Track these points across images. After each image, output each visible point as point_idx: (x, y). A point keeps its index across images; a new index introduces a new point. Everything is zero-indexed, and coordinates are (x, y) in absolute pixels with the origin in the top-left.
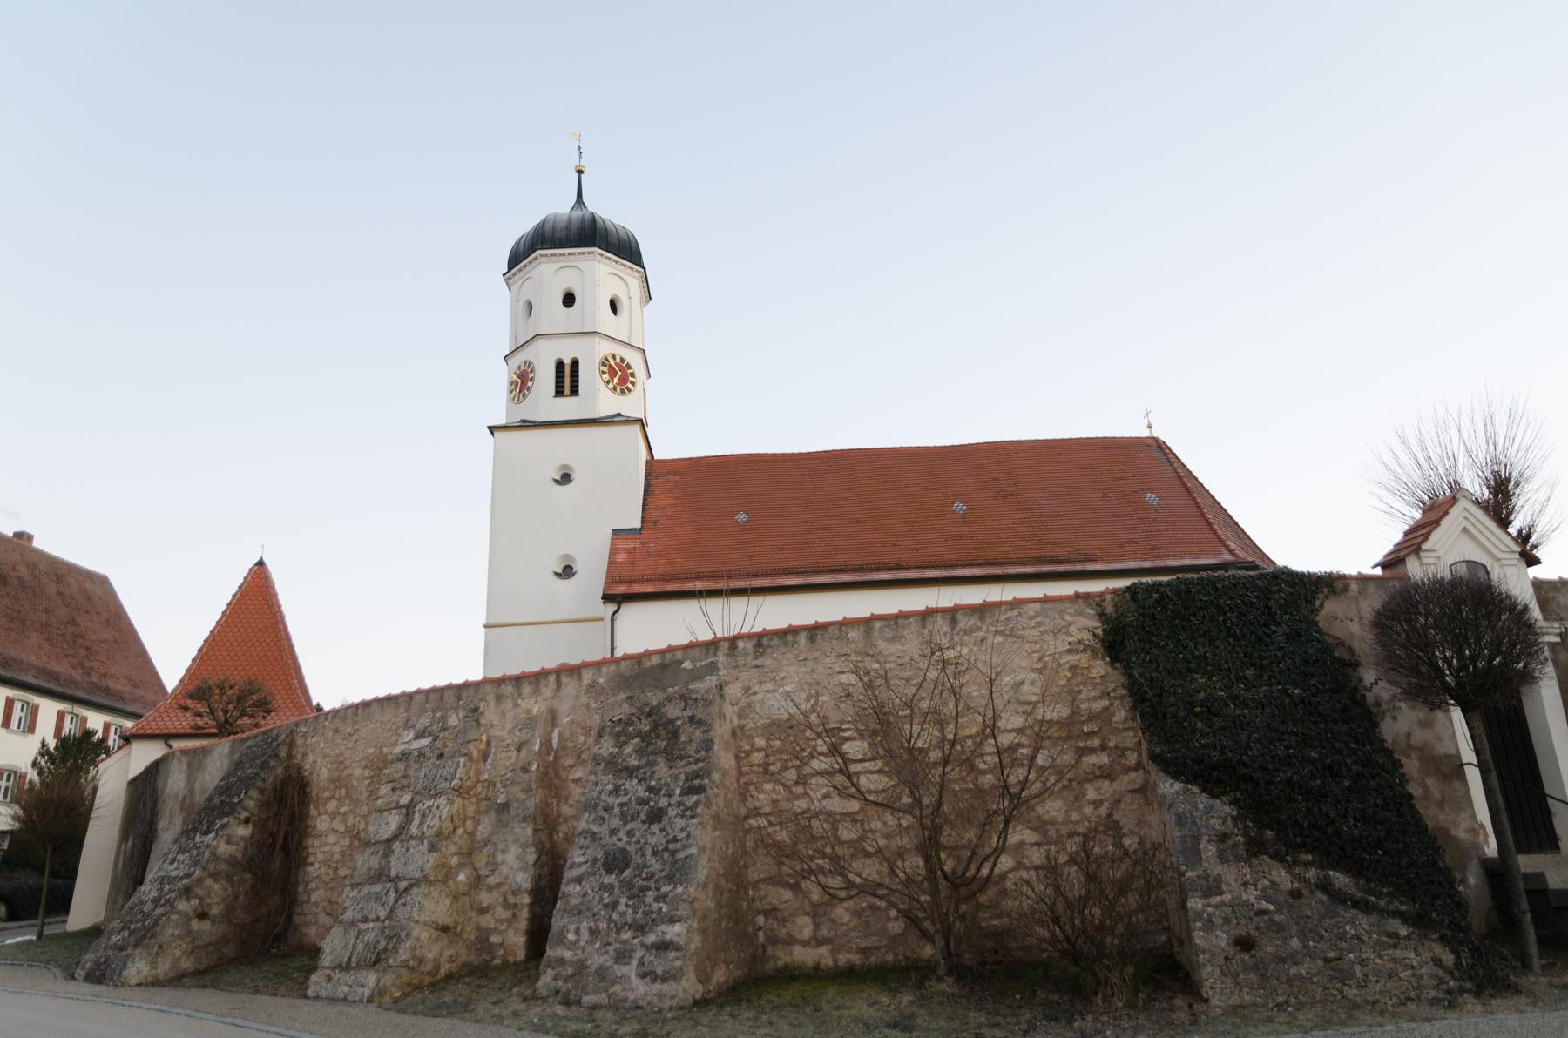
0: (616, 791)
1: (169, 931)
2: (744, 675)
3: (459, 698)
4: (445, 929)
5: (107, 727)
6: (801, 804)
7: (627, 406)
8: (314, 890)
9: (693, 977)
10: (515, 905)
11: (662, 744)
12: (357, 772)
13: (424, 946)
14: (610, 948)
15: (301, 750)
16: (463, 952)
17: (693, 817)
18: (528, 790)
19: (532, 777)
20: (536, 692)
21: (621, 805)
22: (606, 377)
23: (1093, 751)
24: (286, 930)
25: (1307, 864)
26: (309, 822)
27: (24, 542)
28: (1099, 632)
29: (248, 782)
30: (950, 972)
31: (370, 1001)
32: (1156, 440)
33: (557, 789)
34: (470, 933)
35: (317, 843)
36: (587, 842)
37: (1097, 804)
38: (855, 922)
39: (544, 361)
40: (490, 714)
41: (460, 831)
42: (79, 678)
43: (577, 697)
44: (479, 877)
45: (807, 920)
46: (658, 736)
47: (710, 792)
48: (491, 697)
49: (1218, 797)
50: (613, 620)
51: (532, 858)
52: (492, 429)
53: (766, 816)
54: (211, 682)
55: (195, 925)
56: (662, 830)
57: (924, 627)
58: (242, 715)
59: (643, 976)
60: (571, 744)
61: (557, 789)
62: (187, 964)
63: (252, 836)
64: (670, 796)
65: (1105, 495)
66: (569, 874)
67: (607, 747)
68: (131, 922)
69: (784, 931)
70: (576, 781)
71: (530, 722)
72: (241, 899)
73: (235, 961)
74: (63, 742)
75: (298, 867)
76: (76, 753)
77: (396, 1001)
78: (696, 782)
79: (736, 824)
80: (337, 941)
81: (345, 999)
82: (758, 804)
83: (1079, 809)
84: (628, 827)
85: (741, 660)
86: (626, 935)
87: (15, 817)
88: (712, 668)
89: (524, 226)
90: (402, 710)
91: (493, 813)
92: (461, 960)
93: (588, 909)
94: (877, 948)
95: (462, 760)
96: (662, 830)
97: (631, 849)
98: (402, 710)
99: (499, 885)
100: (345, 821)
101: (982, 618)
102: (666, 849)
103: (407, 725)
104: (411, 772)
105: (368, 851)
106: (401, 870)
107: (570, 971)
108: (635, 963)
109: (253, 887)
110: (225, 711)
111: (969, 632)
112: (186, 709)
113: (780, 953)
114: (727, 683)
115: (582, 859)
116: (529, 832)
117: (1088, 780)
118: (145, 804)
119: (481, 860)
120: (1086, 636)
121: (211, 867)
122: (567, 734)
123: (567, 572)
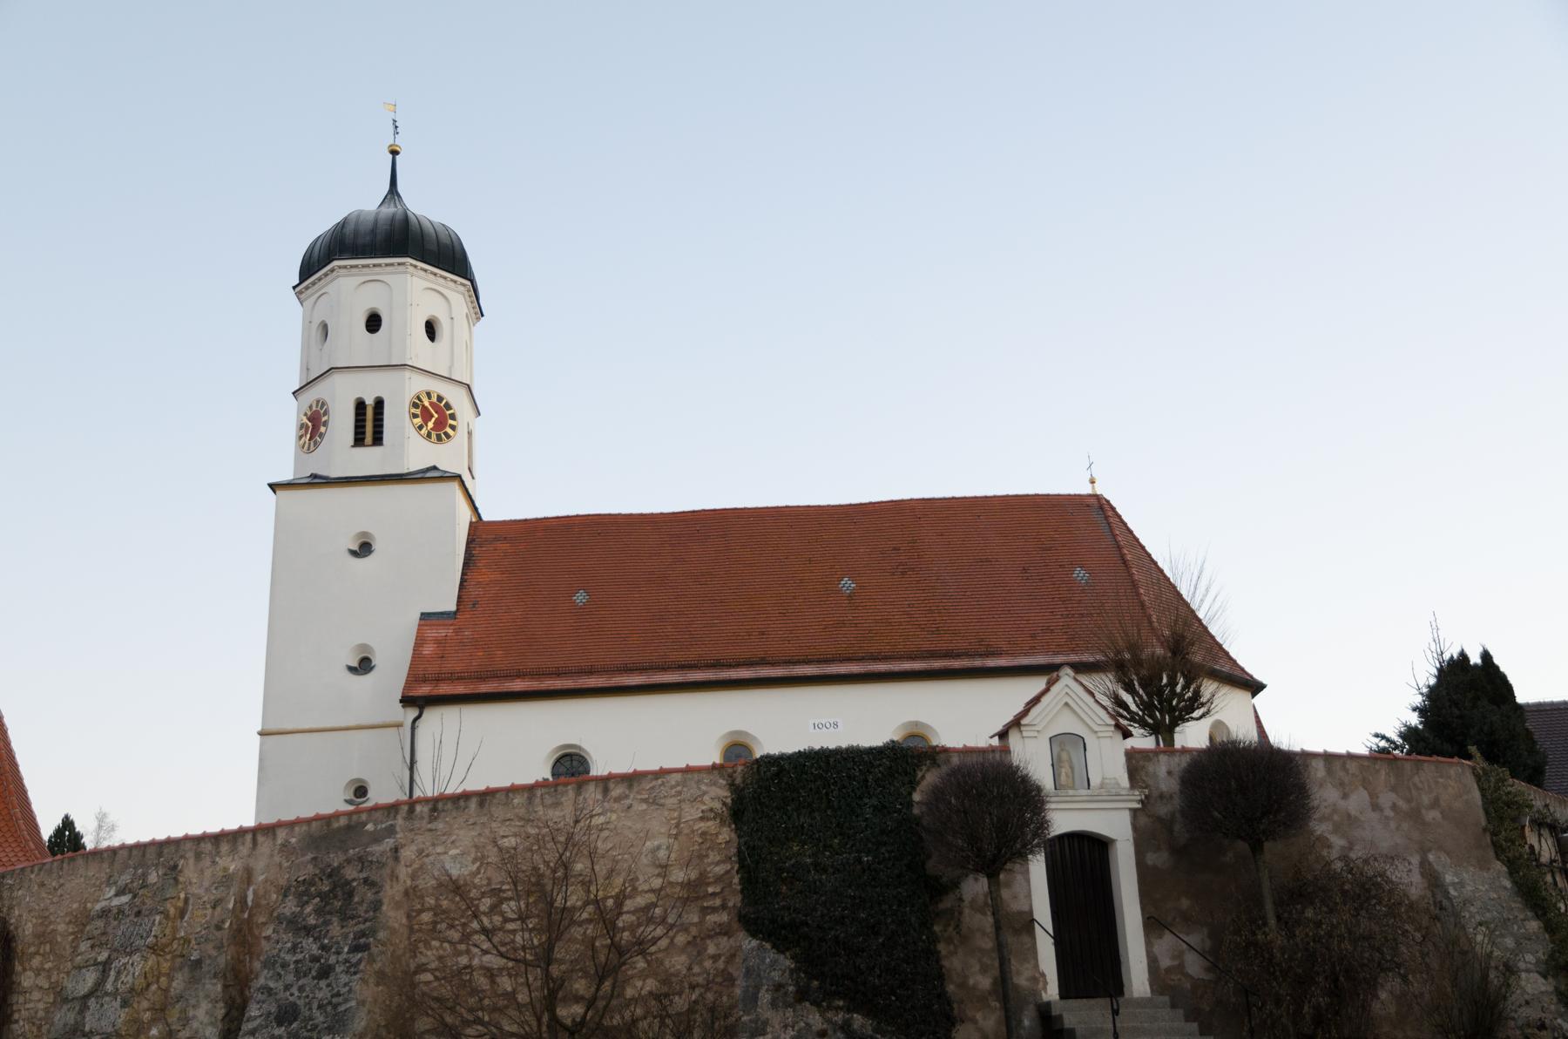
2: (420, 839)
3: (160, 855)
6: (464, 960)
7: (446, 456)
11: (338, 904)
12: (61, 927)
15: (7, 903)
18: (219, 948)
20: (234, 850)
21: (297, 962)
22: (418, 421)
23: (714, 910)
25: (838, 1008)
28: (729, 801)
32: (1098, 497)
35: (21, 999)
37: (715, 958)
39: (341, 400)
40: (189, 872)
41: (154, 987)
44: (170, 1033)
46: (335, 897)
47: (374, 950)
48: (190, 855)
49: (783, 952)
50: (413, 728)
51: (220, 1013)
52: (274, 487)
53: (432, 971)
60: (264, 902)
64: (338, 953)
65: (1025, 570)
70: (268, 938)
71: (226, 880)
78: (362, 941)
79: (403, 981)
82: (424, 960)
83: (700, 963)
85: (417, 824)
88: (391, 831)
89: (321, 224)
90: (105, 865)
91: (186, 969)
95: (158, 918)
97: (301, 1003)
98: (105, 865)
100: (49, 977)
101: (630, 787)
102: (330, 1003)
104: (109, 930)
105: (65, 1007)
111: (618, 800)
114: (403, 846)
115: (257, 1013)
116: (219, 987)
117: (710, 937)
119: (174, 1015)
120: (717, 805)
122: (261, 892)
123: (364, 666)
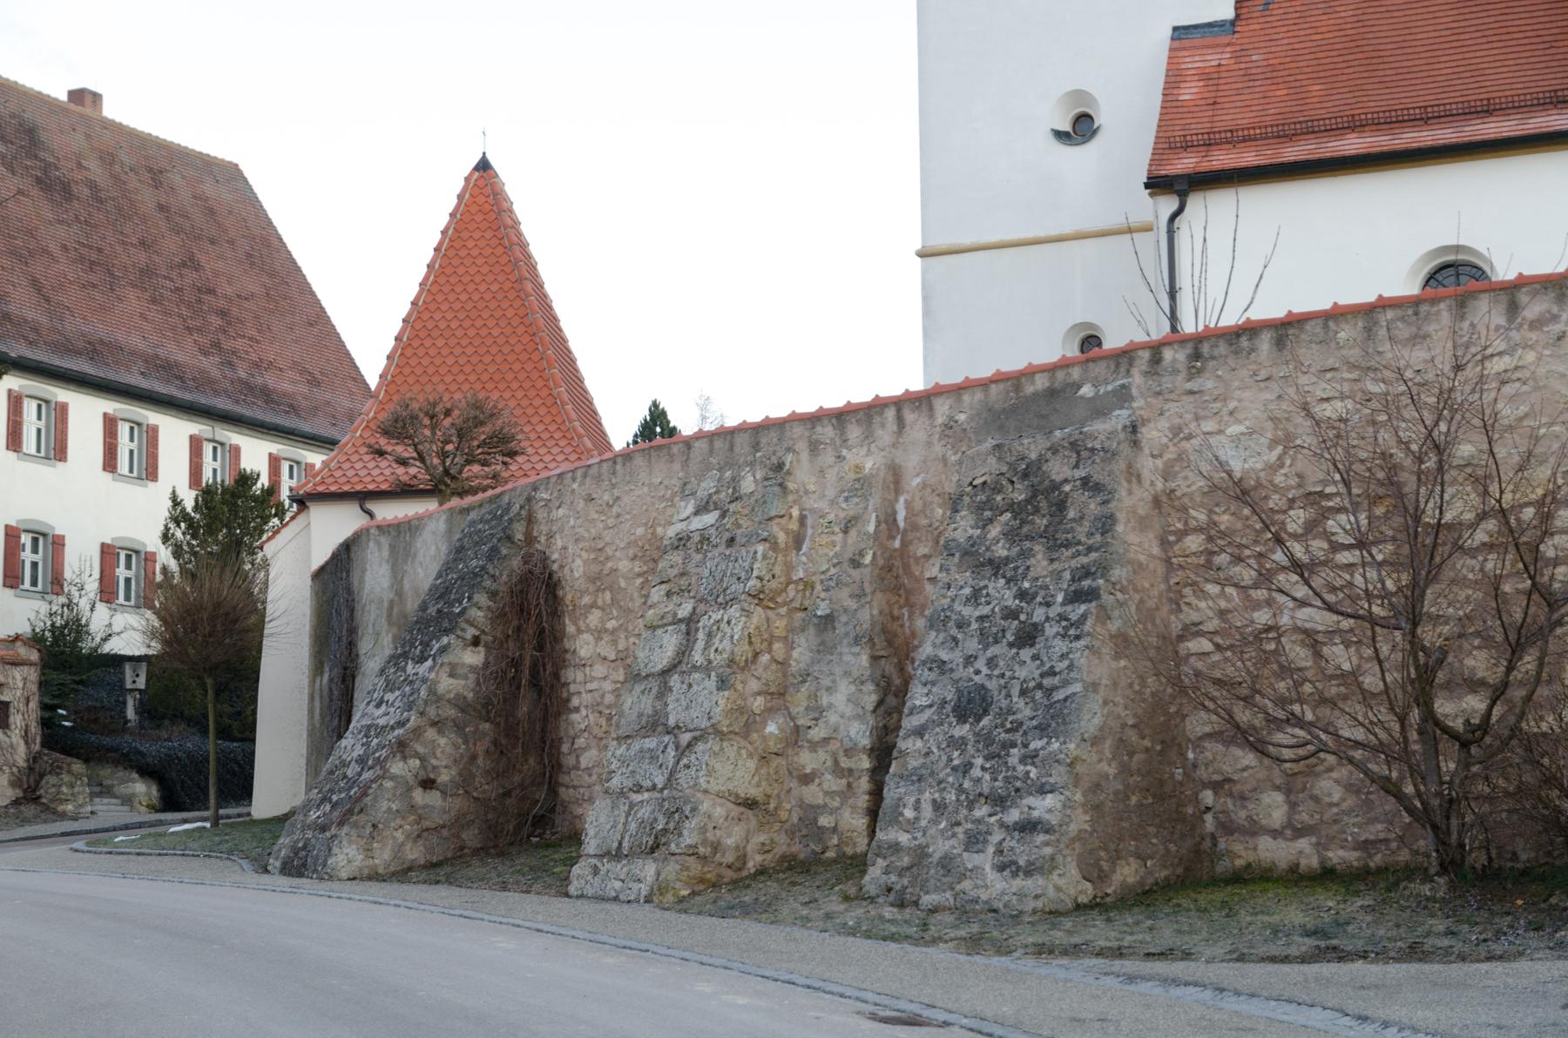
0: (975, 597)
1: (384, 805)
2: (1173, 407)
3: (756, 447)
4: (750, 804)
5: (274, 461)
6: (1262, 617)
8: (585, 749)
9: (1073, 871)
10: (850, 771)
11: (1041, 522)
12: (624, 565)
13: (715, 822)
14: (959, 830)
15: (544, 528)
16: (782, 839)
17: (1078, 638)
19: (865, 574)
20: (868, 437)
21: (981, 618)
24: (552, 810)
26: (567, 644)
27: (87, 110)
29: (472, 580)
30: (1444, 869)
31: (648, 900)
33: (909, 592)
34: (789, 811)
36: (932, 676)
38: (1351, 801)
40: (803, 474)
41: (765, 658)
42: (215, 373)
43: (929, 444)
45: (1279, 797)
46: (1037, 510)
47: (1107, 599)
48: (802, 446)
50: (1171, 233)
54: (415, 406)
55: (419, 796)
56: (1035, 657)
57: (1463, 318)
58: (468, 462)
59: (1001, 868)
61: (909, 592)
62: (414, 853)
63: (486, 664)
64: (1048, 605)
66: (910, 723)
67: (964, 528)
68: (332, 791)
69: (1243, 814)
71: (860, 486)
72: (480, 761)
73: (481, 852)
74: (207, 496)
75: (559, 714)
76: (228, 518)
77: (681, 900)
78: (1086, 583)
80: (602, 819)
81: (616, 899)
84: (989, 653)
85: (1167, 382)
86: (981, 811)
87: (152, 634)
88: (1123, 396)
90: (677, 466)
91: (812, 631)
92: (780, 850)
93: (932, 774)
94: (1386, 841)
95: (760, 548)
96: (1035, 657)
97: (992, 685)
98: (677, 466)
99: (826, 740)
100: (615, 642)
102: (1039, 686)
103: (685, 491)
104: (691, 568)
105: (638, 688)
106: (682, 716)
107: (906, 861)
108: (991, 850)
109: (495, 743)
110: (443, 455)
111: (1536, 324)
112: (381, 453)
113: (1238, 848)
114: (1145, 422)
115: (924, 701)
116: (864, 659)
118: (339, 614)
119: (799, 701)
121: (432, 712)
122: (918, 504)
123: (1081, 128)
